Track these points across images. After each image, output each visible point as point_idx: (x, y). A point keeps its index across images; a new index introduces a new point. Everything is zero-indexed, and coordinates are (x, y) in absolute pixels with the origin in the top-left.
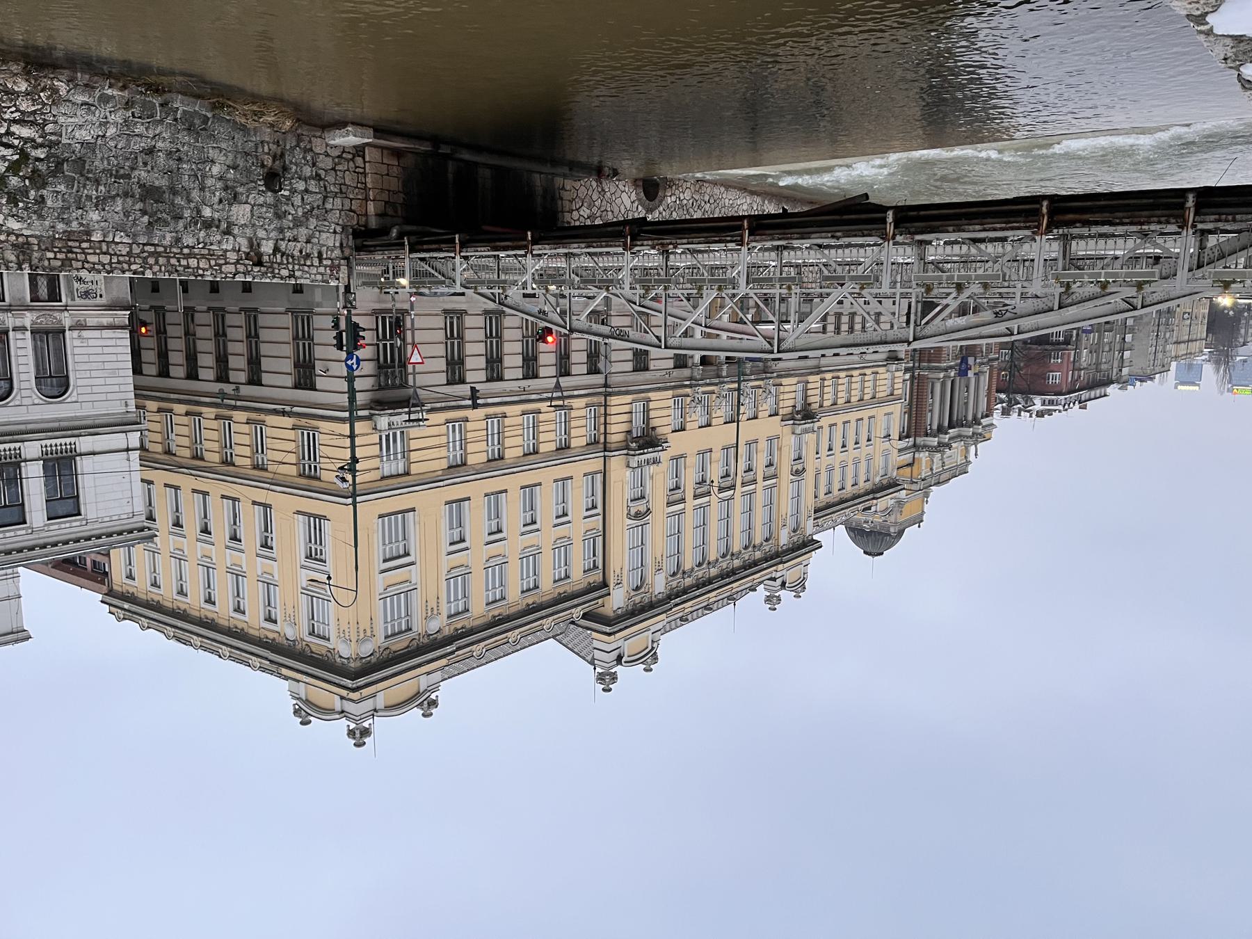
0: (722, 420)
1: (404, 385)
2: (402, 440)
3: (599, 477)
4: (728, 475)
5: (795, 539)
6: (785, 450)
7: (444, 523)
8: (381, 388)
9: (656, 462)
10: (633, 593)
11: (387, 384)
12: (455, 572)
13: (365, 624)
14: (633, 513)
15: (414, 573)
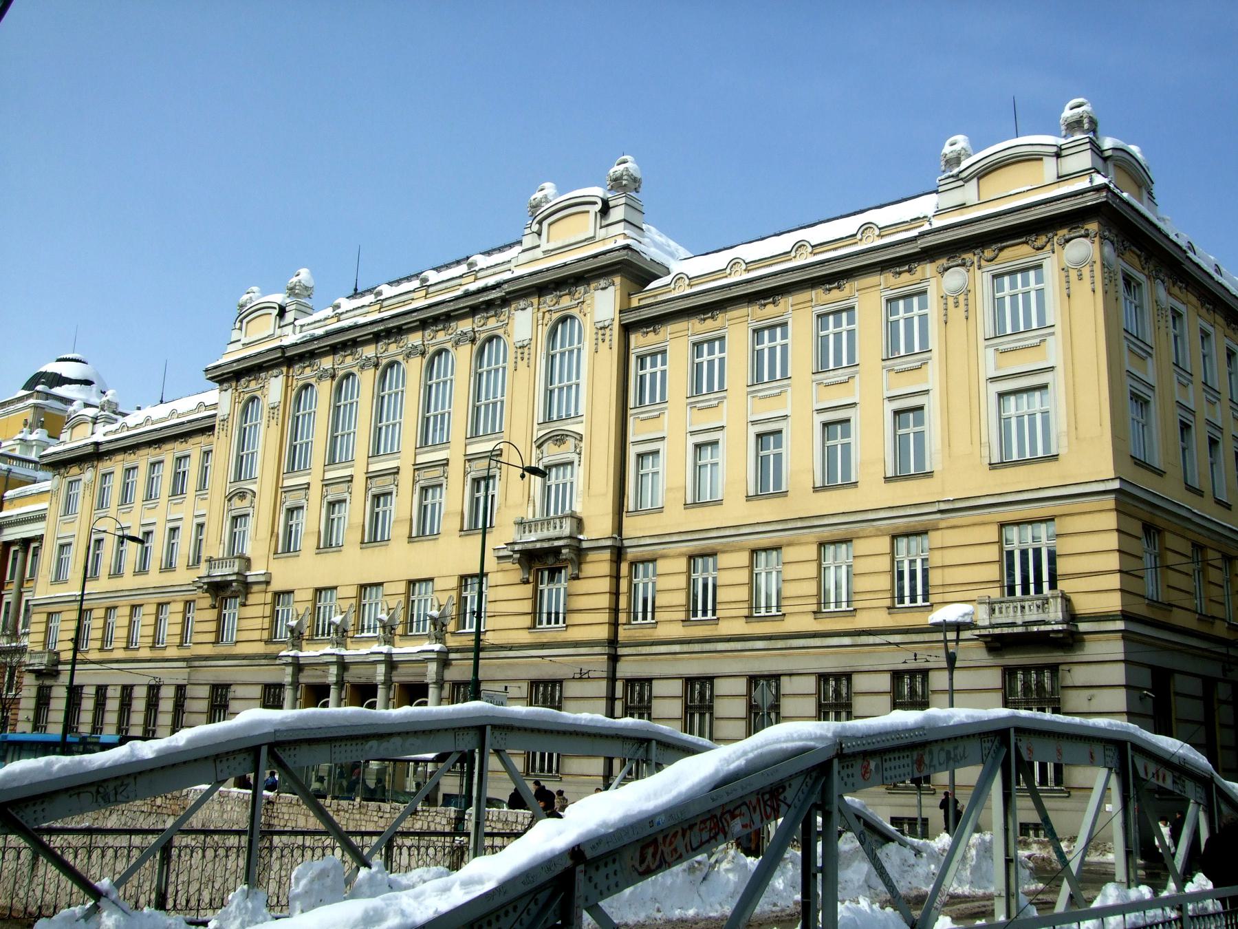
0: (388, 589)
1: (1009, 673)
2: (901, 589)
3: (630, 503)
4: (291, 511)
5: (253, 385)
6: (265, 531)
7: (934, 442)
8: (1054, 668)
9: (521, 524)
10: (258, 394)
11: (912, 678)
12: (841, 375)
13: (957, 315)
14: (570, 442)
15: (989, 363)
